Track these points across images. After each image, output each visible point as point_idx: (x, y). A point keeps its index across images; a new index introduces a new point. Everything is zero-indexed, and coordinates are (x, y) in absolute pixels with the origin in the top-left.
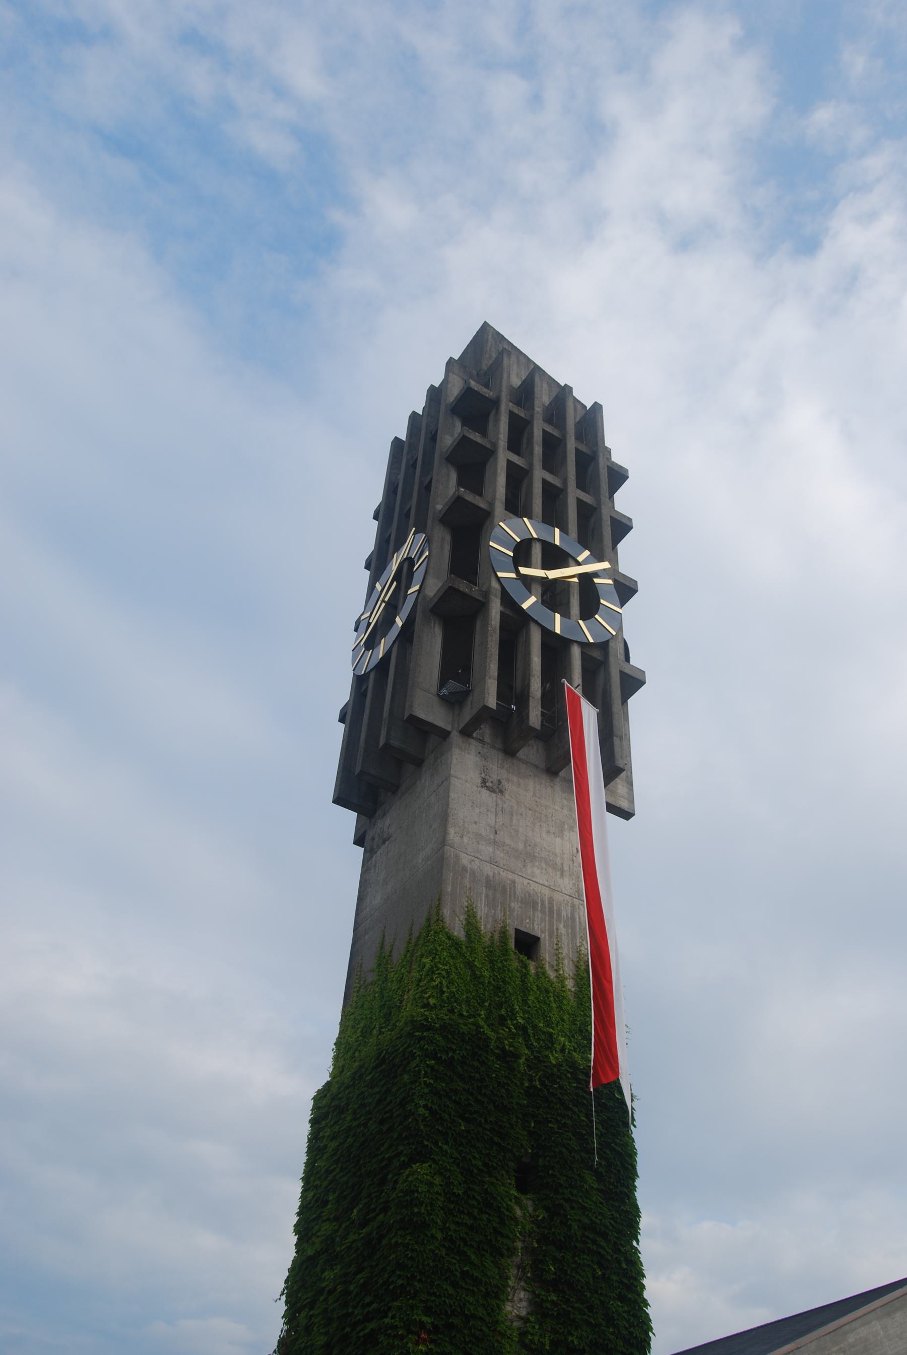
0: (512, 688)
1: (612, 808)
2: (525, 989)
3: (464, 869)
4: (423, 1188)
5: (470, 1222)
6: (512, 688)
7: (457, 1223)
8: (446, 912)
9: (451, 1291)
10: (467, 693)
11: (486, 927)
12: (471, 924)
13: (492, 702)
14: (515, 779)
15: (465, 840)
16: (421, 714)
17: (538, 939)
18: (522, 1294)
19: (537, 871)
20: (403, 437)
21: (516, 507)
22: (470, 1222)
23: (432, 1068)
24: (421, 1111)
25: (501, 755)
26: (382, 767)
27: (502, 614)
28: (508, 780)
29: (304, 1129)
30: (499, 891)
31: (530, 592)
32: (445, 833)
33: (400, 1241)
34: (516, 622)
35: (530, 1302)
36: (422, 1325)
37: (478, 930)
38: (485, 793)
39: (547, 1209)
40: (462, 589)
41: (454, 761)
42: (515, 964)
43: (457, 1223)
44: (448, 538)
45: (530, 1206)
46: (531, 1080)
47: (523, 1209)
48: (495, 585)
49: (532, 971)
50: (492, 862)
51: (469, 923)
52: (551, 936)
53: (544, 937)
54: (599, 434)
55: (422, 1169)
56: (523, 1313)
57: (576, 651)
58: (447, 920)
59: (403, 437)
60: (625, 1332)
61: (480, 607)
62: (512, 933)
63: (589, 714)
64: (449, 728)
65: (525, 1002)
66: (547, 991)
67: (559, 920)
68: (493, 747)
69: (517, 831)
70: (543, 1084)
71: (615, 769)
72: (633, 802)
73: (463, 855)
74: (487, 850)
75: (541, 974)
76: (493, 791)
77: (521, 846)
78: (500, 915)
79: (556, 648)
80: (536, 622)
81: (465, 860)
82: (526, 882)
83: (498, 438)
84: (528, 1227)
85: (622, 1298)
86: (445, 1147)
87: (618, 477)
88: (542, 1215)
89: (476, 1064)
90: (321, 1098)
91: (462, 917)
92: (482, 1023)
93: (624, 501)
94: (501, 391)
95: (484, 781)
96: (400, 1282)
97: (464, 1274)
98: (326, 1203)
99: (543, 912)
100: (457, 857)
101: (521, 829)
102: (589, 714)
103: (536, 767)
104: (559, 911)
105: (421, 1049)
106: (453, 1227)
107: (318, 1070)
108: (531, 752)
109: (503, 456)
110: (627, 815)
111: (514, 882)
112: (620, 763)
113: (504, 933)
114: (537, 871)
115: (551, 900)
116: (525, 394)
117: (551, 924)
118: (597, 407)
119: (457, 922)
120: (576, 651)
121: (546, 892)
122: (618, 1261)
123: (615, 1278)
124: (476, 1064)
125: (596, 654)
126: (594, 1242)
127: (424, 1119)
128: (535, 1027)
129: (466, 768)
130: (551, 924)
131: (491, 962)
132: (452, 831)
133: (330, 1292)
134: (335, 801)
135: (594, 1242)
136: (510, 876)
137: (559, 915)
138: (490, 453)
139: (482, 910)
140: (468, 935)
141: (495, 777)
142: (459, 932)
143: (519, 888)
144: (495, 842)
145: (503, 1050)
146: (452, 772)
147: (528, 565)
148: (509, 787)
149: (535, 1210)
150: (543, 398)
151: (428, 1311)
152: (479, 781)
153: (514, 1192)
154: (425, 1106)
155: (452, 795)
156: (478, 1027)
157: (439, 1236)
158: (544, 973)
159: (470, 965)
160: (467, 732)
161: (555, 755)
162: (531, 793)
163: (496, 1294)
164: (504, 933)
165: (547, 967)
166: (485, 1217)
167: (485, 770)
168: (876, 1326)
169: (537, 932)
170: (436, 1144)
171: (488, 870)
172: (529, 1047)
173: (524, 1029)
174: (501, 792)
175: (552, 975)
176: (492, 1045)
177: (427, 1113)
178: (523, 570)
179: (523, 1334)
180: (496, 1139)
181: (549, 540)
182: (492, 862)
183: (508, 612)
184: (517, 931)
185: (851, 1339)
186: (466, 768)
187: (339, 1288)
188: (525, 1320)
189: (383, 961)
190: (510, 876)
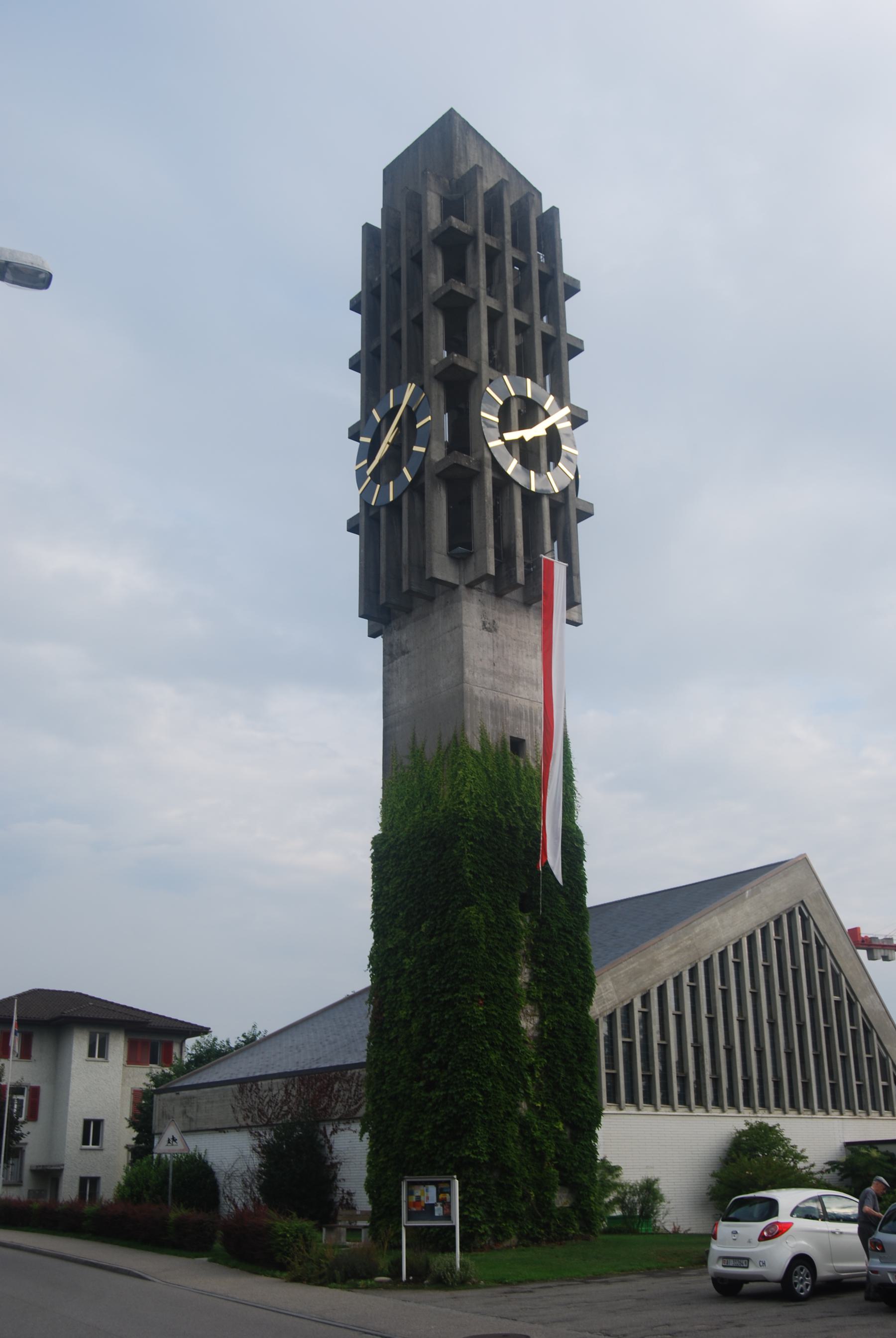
0: (505, 556)
1: (569, 622)
2: (519, 780)
3: (477, 699)
4: (474, 922)
5: (499, 937)
6: (505, 556)
7: (493, 939)
8: (468, 734)
9: (493, 977)
10: (470, 554)
11: (492, 739)
12: (484, 740)
13: (492, 571)
14: (503, 616)
15: (476, 675)
16: (438, 575)
17: (524, 741)
18: (526, 970)
19: (521, 689)
20: (377, 223)
21: (498, 364)
22: (499, 937)
23: (471, 846)
24: (468, 875)
25: (494, 597)
26: (399, 590)
27: (493, 478)
28: (499, 619)
29: (368, 865)
30: (498, 709)
31: (511, 454)
32: (463, 674)
33: (463, 952)
34: (503, 482)
35: (530, 974)
36: (479, 996)
37: (488, 742)
38: (485, 633)
39: (538, 921)
40: (463, 464)
41: (464, 612)
42: (511, 762)
43: (493, 939)
44: (442, 394)
45: (527, 918)
46: (526, 843)
47: (524, 921)
48: (487, 455)
49: (522, 765)
50: (493, 689)
51: (482, 739)
52: (532, 737)
53: (528, 738)
54: (558, 249)
55: (473, 910)
56: (527, 980)
57: (546, 503)
58: (469, 740)
59: (377, 223)
60: (582, 986)
61: (476, 475)
62: (508, 740)
63: (560, 570)
64: (457, 583)
65: (519, 789)
66: (532, 778)
67: (536, 724)
68: (488, 593)
69: (507, 660)
70: (533, 844)
71: (573, 601)
72: (581, 614)
73: (475, 688)
74: (490, 679)
75: (528, 766)
76: (491, 631)
77: (510, 671)
78: (500, 728)
79: (531, 499)
80: (517, 484)
81: (477, 691)
82: (515, 699)
83: (479, 286)
84: (528, 933)
85: (580, 967)
86: (483, 895)
87: (572, 289)
88: (536, 925)
89: (495, 839)
90: (377, 842)
91: (478, 736)
92: (496, 811)
93: (577, 318)
94: (477, 225)
95: (484, 624)
96: (465, 974)
97: (499, 966)
98: (396, 916)
99: (526, 720)
100: (472, 690)
101: (510, 658)
102: (560, 570)
103: (517, 602)
104: (536, 716)
105: (464, 834)
106: (491, 941)
107: (371, 824)
108: (516, 594)
109: (486, 302)
110: (576, 624)
111: (507, 701)
112: (577, 600)
113: (504, 741)
114: (521, 689)
115: (531, 709)
116: (494, 198)
117: (531, 726)
118: (554, 211)
119: (475, 739)
120: (546, 503)
121: (528, 704)
122: (578, 946)
123: (576, 956)
124: (495, 839)
125: (560, 499)
126: (565, 937)
127: (470, 879)
128: (526, 805)
129: (472, 611)
130: (531, 726)
131: (498, 765)
132: (467, 670)
133: (411, 973)
134: (360, 616)
135: (565, 937)
136: (505, 697)
137: (536, 719)
138: (474, 302)
139: (489, 727)
140: (482, 748)
141: (491, 618)
142: (477, 747)
143: (510, 703)
144: (494, 672)
145: (510, 827)
146: (464, 622)
147: (509, 430)
148: (500, 624)
149: (531, 921)
150: (509, 201)
151: (482, 989)
152: (481, 624)
153: (519, 914)
154: (470, 872)
155: (465, 641)
156: (495, 814)
157: (484, 947)
158: (529, 766)
159: (486, 770)
160: (470, 586)
161: (534, 595)
162: (515, 626)
163: (514, 973)
164: (504, 741)
165: (530, 760)
166: (507, 933)
167: (484, 614)
168: (716, 920)
169: (523, 737)
170: (478, 894)
171: (491, 695)
172: (524, 820)
173: (519, 808)
174: (496, 630)
175: (533, 765)
176: (504, 826)
177: (471, 876)
178: (508, 436)
179: (528, 992)
180: (510, 885)
181: (522, 394)
182: (493, 689)
183: (496, 476)
184: (511, 737)
185: (697, 930)
186: (472, 611)
187: (418, 971)
188: (529, 984)
189: (416, 753)
190: (505, 697)
